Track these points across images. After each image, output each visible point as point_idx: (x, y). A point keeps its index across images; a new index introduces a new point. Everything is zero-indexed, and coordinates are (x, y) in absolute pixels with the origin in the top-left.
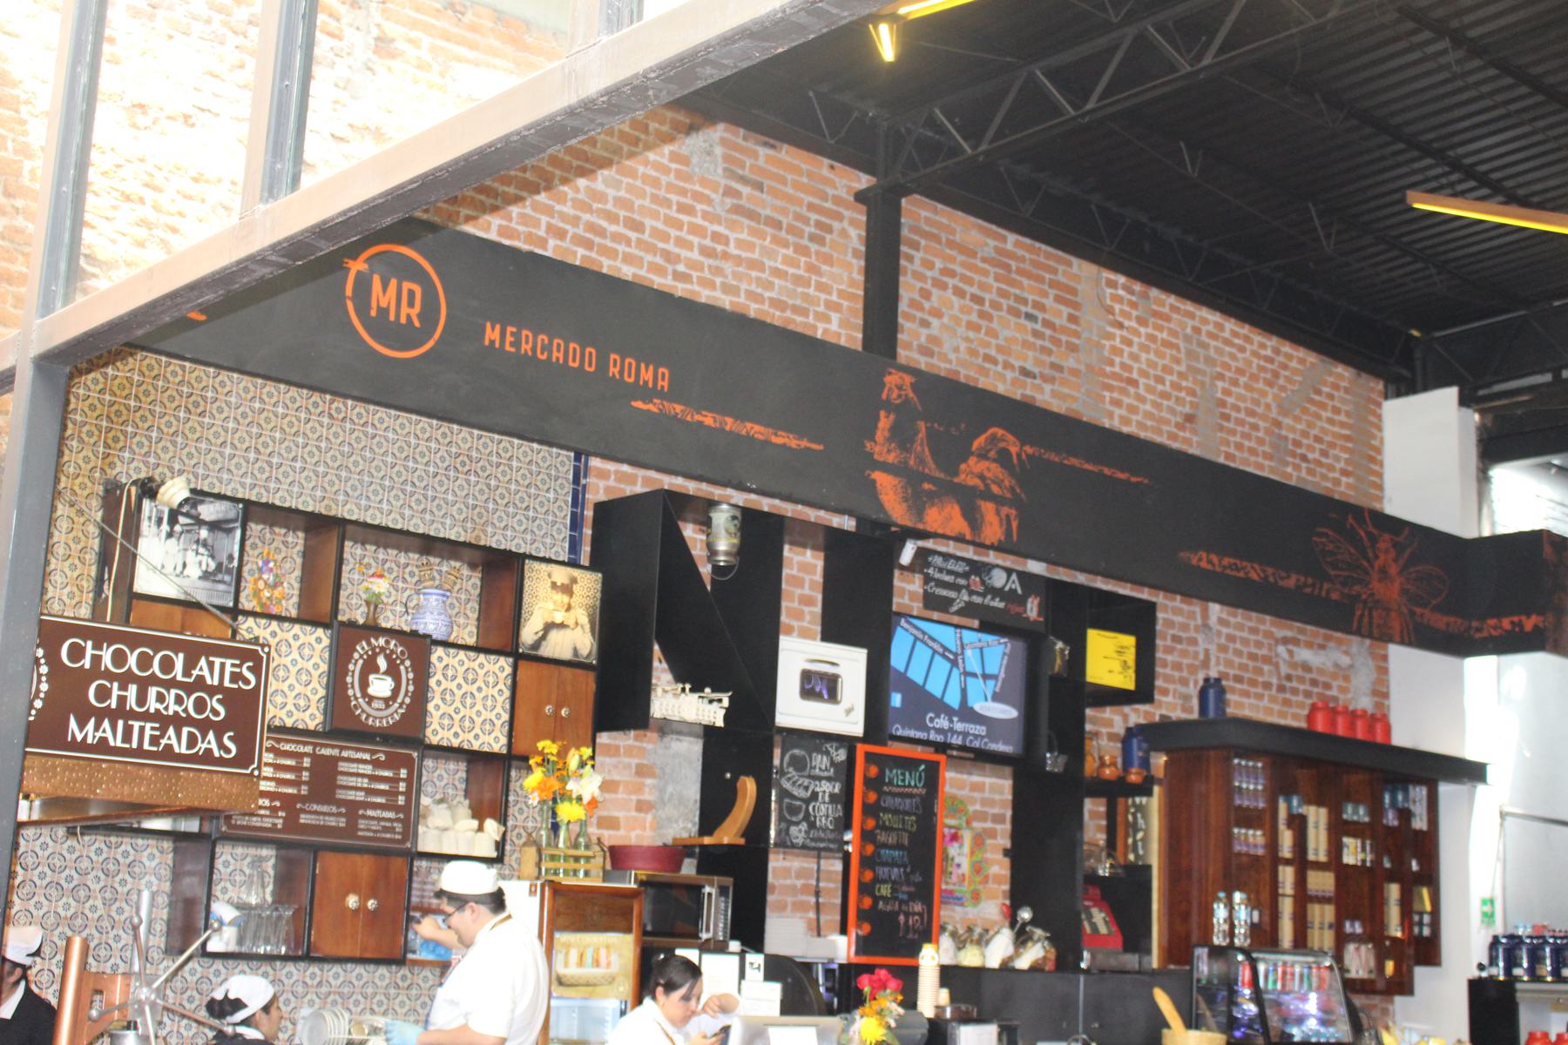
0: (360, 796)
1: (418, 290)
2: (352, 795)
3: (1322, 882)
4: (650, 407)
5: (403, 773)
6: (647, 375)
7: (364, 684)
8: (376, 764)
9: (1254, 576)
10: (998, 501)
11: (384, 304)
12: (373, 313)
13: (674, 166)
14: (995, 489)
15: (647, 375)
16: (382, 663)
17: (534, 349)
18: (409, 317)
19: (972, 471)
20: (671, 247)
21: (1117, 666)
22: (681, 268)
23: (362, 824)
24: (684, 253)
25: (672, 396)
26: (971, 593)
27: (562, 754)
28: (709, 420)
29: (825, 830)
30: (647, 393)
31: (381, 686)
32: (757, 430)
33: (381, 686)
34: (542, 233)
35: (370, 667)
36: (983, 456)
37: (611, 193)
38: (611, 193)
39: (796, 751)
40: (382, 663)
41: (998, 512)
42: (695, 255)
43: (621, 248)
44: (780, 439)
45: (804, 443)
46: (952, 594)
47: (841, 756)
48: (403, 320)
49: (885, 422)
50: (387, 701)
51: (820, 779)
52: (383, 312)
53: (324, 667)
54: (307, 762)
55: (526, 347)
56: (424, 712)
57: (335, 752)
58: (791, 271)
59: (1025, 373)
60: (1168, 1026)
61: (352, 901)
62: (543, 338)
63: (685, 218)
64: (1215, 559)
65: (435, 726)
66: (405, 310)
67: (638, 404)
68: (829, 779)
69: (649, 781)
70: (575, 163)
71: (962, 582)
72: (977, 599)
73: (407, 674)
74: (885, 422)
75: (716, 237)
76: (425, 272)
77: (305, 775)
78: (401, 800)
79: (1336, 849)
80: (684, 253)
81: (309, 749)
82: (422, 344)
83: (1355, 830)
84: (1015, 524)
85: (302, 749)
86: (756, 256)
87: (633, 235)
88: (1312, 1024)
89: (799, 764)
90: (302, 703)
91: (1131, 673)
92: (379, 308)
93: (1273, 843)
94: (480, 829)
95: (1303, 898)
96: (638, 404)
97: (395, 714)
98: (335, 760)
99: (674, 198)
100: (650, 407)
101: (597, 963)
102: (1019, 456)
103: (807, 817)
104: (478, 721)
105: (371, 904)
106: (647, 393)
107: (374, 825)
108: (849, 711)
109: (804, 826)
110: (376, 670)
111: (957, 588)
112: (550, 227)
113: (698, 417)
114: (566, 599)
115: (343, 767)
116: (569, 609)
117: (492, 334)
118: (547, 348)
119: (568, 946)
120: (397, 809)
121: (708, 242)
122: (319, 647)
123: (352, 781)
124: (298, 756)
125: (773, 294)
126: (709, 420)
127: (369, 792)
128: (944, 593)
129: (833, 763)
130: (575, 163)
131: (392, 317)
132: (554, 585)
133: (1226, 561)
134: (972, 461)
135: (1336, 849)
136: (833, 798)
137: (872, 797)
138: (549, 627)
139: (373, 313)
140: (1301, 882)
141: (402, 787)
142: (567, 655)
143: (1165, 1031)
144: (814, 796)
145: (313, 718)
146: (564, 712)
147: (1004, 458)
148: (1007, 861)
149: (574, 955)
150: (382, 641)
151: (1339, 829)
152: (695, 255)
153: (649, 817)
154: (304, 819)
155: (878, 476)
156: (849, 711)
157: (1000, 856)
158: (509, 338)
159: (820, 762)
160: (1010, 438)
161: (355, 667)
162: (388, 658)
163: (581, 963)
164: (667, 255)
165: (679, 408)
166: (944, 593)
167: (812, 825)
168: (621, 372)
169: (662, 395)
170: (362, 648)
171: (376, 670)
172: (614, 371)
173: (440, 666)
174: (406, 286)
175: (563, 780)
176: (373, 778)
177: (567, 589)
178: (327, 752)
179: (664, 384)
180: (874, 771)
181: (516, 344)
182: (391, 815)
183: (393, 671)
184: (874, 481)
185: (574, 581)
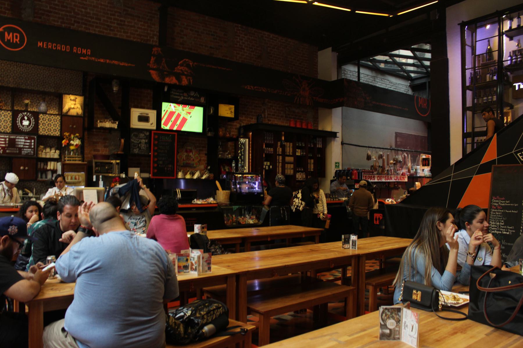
0: (22, 146)
1: (18, 35)
2: (20, 146)
3: (291, 159)
4: (86, 59)
5: (33, 141)
6: (84, 51)
7: (21, 123)
8: (26, 139)
9: (264, 91)
10: (187, 76)
11: (9, 38)
12: (6, 40)
13: (109, 5)
14: (185, 73)
15: (84, 51)
16: (26, 118)
17: (52, 47)
18: (16, 41)
19: (179, 69)
20: (109, 24)
21: (229, 112)
22: (112, 28)
23: (23, 152)
24: (112, 25)
25: (91, 56)
26: (184, 97)
27: (70, 136)
28: (102, 61)
29: (144, 150)
30: (84, 55)
31: (26, 123)
32: (116, 62)
33: (26, 123)
34: (73, 22)
35: (23, 119)
36: (182, 65)
37: (92, 12)
38: (92, 12)
39: (135, 133)
40: (26, 118)
41: (186, 78)
42: (115, 25)
43: (95, 25)
44: (122, 64)
45: (129, 65)
46: (179, 97)
47: (148, 134)
48: (15, 42)
49: (153, 59)
50: (28, 126)
51: (142, 139)
52: (9, 40)
53: (11, 119)
54: (7, 139)
55: (50, 47)
56: (38, 128)
57: (15, 137)
58: (143, 27)
59: (211, 47)
60: (218, 190)
61: (22, 168)
62: (54, 44)
63: (112, 17)
64: (252, 87)
65: (41, 130)
66: (15, 40)
67: (82, 58)
68: (144, 139)
69: (107, 141)
70: (81, 6)
71: (181, 94)
72: (185, 98)
73: (32, 119)
74: (153, 59)
75: (121, 21)
76: (20, 31)
77: (7, 142)
78: (33, 147)
79: (294, 152)
80: (112, 25)
81: (8, 137)
82: (19, 48)
83: (299, 148)
84: (191, 81)
85: (6, 137)
86: (133, 24)
87: (98, 22)
88: (257, 189)
89: (136, 136)
90: (6, 127)
91: (233, 114)
92: (7, 39)
93: (275, 150)
94: (55, 152)
95: (284, 163)
96: (82, 58)
97: (30, 128)
98: (14, 139)
99: (109, 12)
100: (86, 59)
101: (76, 179)
102: (193, 65)
103: (138, 147)
104: (52, 129)
105: (26, 168)
106: (84, 55)
107: (26, 152)
108: (152, 124)
109: (138, 149)
110: (25, 119)
111: (180, 96)
112: (75, 21)
113: (99, 60)
114: (74, 102)
115: (17, 140)
116: (75, 104)
117: (40, 44)
118: (56, 47)
119: (68, 176)
120: (32, 149)
121: (119, 22)
122: (9, 115)
123: (20, 143)
124: (5, 138)
125: (138, 33)
126: (102, 61)
127: (24, 145)
128: (176, 97)
129: (145, 135)
130: (81, 6)
131: (11, 41)
132: (71, 100)
133: (255, 87)
134: (178, 67)
135: (294, 152)
136: (145, 143)
137: (156, 142)
138: (69, 109)
139: (6, 40)
140: (283, 159)
141: (33, 144)
142: (75, 114)
143: (217, 191)
144: (140, 143)
145: (9, 130)
146: (75, 126)
147: (188, 66)
148: (206, 157)
149: (69, 178)
150: (25, 113)
151: (295, 148)
152: (115, 25)
153: (107, 149)
154: (7, 151)
155: (152, 72)
156: (152, 124)
157: (204, 155)
158: (45, 45)
159: (142, 135)
160: (190, 61)
161: (19, 119)
162: (27, 117)
163: (71, 179)
164: (108, 26)
165: (93, 58)
166: (176, 97)
167: (140, 149)
168: (77, 51)
169: (88, 56)
170: (20, 115)
171: (25, 119)
172: (75, 51)
173: (41, 118)
174: (15, 34)
175: (69, 141)
176: (25, 142)
177: (75, 100)
178: (12, 137)
179: (89, 53)
180: (156, 137)
181: (47, 46)
182: (30, 150)
183: (29, 119)
184: (150, 73)
185: (76, 98)
